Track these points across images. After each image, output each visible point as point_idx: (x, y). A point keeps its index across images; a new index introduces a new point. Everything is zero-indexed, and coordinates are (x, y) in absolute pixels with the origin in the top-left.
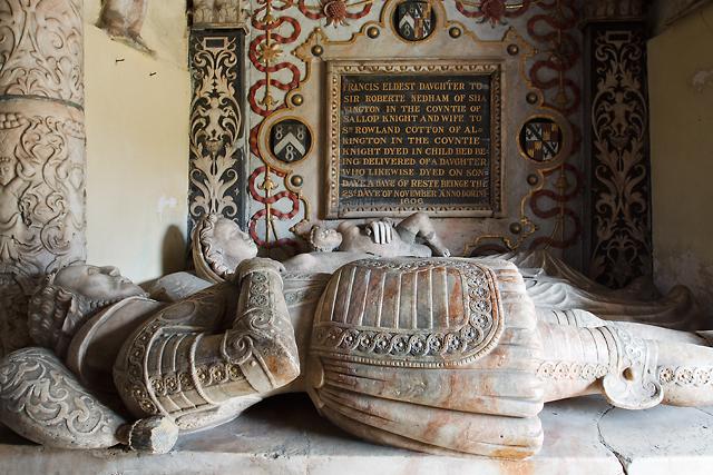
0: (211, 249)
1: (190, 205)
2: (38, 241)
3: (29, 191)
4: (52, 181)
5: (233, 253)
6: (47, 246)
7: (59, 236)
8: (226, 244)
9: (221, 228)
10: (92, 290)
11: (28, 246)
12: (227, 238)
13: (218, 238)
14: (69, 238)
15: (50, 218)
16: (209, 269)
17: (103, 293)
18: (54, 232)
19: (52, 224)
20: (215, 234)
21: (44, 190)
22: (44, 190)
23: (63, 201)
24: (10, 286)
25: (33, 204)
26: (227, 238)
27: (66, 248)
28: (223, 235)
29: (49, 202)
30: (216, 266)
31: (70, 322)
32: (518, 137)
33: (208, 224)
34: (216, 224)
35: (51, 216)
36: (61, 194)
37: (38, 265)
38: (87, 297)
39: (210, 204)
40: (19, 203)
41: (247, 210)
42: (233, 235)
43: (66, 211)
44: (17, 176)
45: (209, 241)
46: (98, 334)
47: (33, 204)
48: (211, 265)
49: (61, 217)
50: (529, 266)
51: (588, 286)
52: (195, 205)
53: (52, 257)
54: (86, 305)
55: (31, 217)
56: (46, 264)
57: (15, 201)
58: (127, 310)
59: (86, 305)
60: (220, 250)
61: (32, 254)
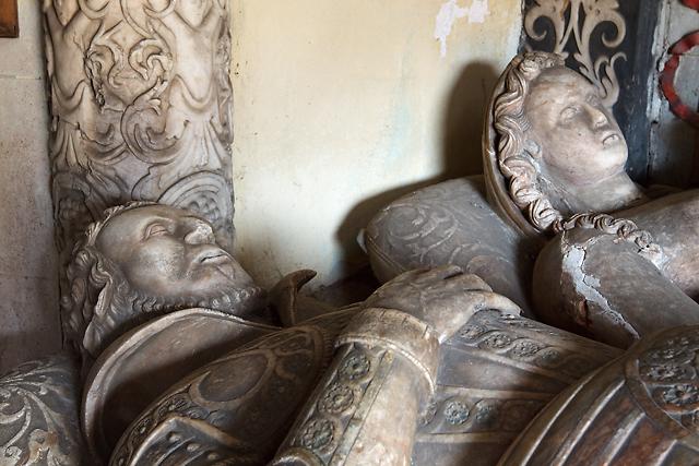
0: (512, 144)
1: (525, 12)
2: (118, 137)
3: (99, 40)
4: (140, 17)
5: (561, 160)
6: (136, 147)
7: (157, 127)
8: (548, 136)
9: (542, 97)
10: (143, 274)
11: (101, 146)
12: (552, 120)
13: (531, 122)
14: (176, 129)
15: (138, 91)
16: (502, 191)
17: (155, 283)
18: (146, 119)
19: (140, 105)
20: (526, 109)
21: (126, 36)
22: (126, 36)
23: (163, 58)
24: (80, 213)
25: (106, 65)
26: (552, 120)
27: (171, 148)
28: (544, 114)
29: (133, 62)
30: (515, 186)
31: (93, 334)
32: (499, 219)
33: (514, 84)
34: (534, 84)
35: (141, 87)
36: (159, 42)
37: (120, 181)
38: (134, 287)
39: (567, 15)
40: (86, 59)
41: (661, 29)
42: (569, 114)
43: (168, 76)
44: (79, 10)
45: (512, 126)
46: (131, 368)
47: (106, 65)
48: (508, 181)
49: (160, 89)
50: (504, 401)
51: (607, 430)
52: (535, 14)
53: (142, 168)
54: (125, 305)
55: (104, 91)
56: (132, 179)
57: (80, 57)
58: (180, 332)
59: (125, 305)
60: (534, 149)
61: (106, 161)
